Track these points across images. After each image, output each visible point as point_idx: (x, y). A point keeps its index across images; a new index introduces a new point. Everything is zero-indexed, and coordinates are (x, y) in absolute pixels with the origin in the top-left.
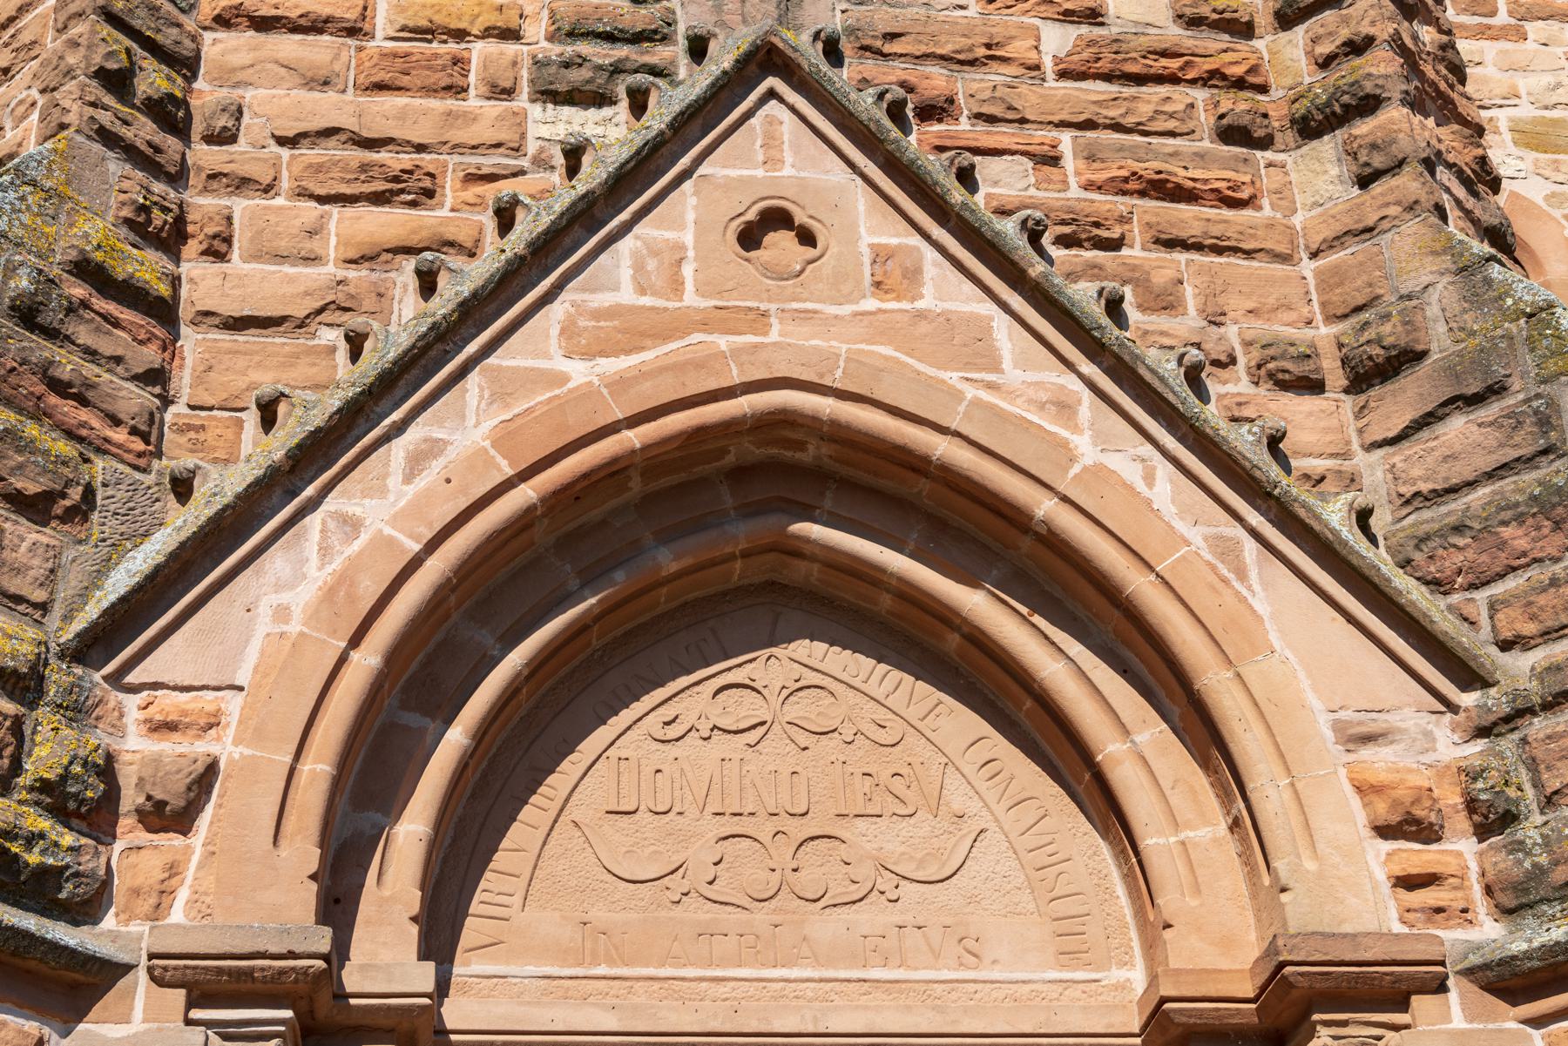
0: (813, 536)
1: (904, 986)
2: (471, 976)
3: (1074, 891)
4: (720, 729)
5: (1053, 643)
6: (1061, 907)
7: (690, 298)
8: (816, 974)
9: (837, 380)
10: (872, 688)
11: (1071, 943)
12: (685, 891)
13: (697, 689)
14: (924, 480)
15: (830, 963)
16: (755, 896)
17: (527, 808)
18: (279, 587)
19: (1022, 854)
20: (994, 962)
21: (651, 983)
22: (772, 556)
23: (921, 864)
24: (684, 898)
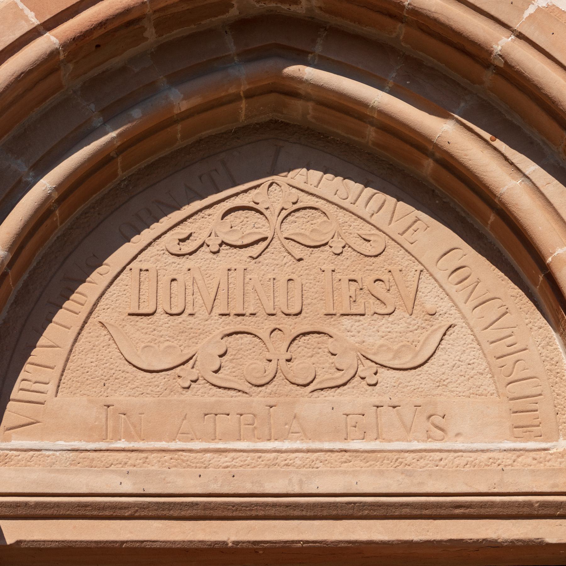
0: (305, 77)
1: (379, 455)
2: (11, 450)
3: (529, 375)
4: (227, 244)
5: (512, 164)
6: (516, 389)
8: (304, 446)
10: (359, 208)
11: (524, 419)
12: (194, 378)
13: (208, 211)
14: (400, 25)
15: (317, 436)
16: (254, 382)
17: (61, 312)
19: (485, 345)
20: (458, 435)
21: (164, 454)
22: (272, 97)
23: (397, 354)
24: (193, 385)
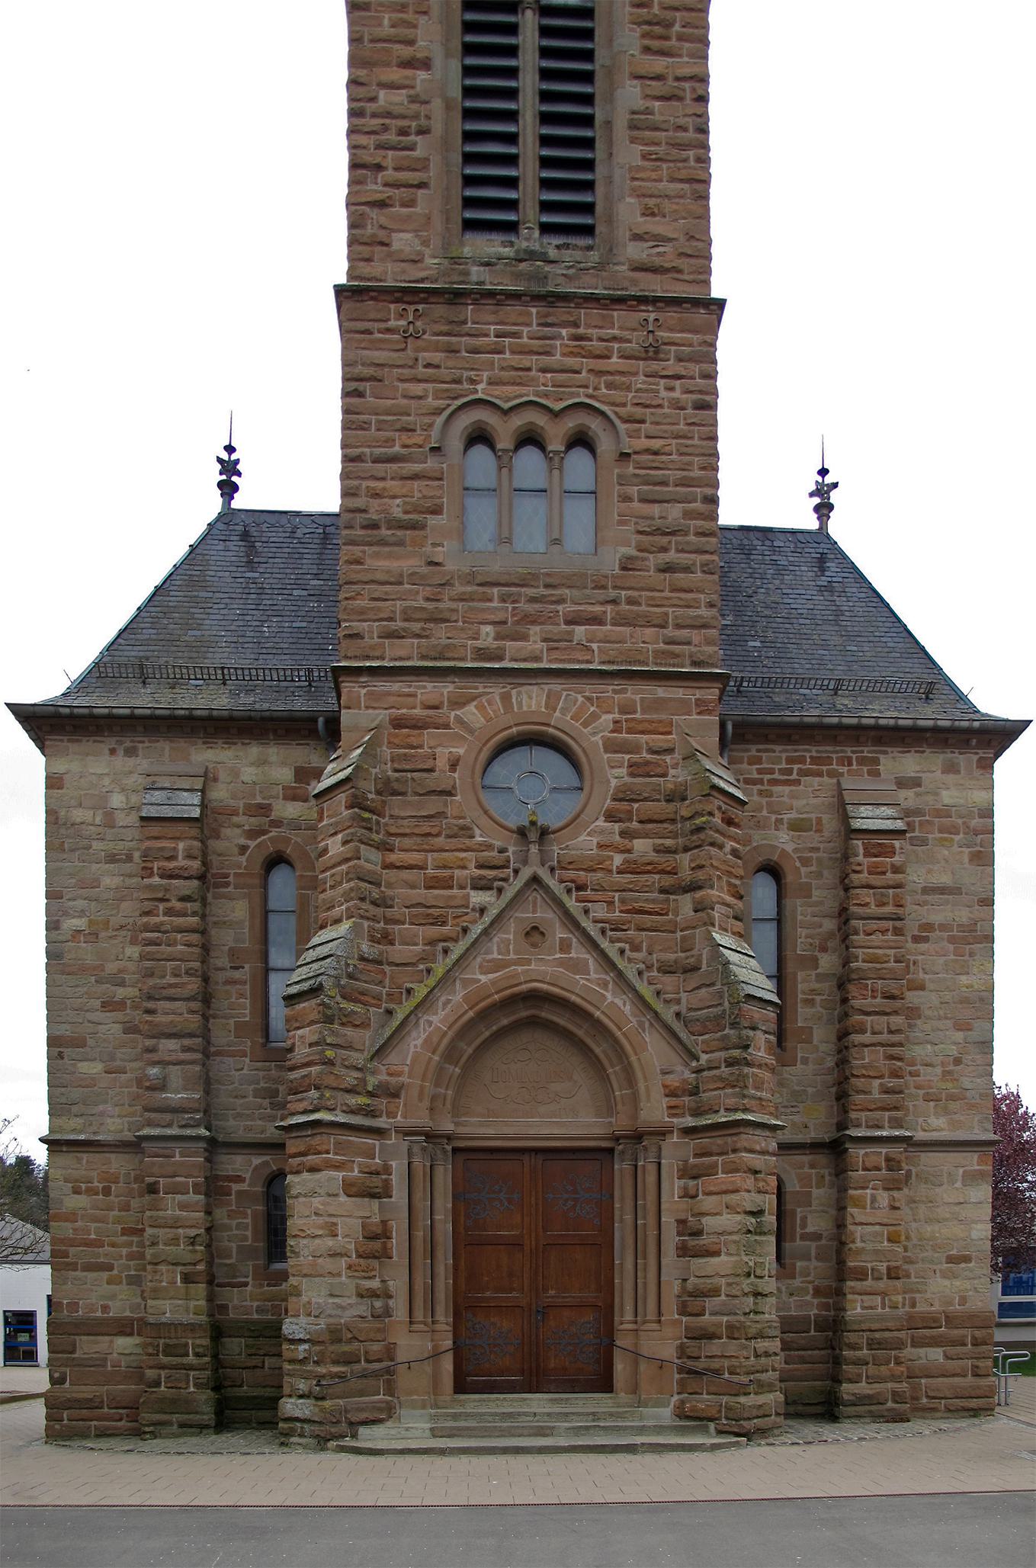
7: (512, 956)
9: (548, 979)
18: (414, 1040)
